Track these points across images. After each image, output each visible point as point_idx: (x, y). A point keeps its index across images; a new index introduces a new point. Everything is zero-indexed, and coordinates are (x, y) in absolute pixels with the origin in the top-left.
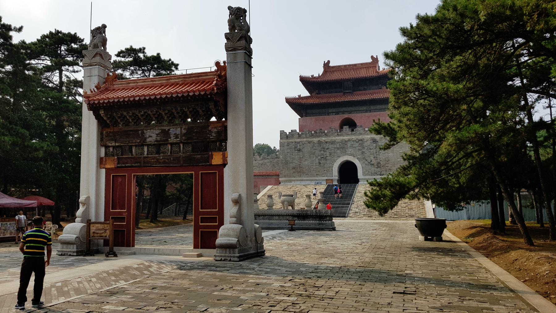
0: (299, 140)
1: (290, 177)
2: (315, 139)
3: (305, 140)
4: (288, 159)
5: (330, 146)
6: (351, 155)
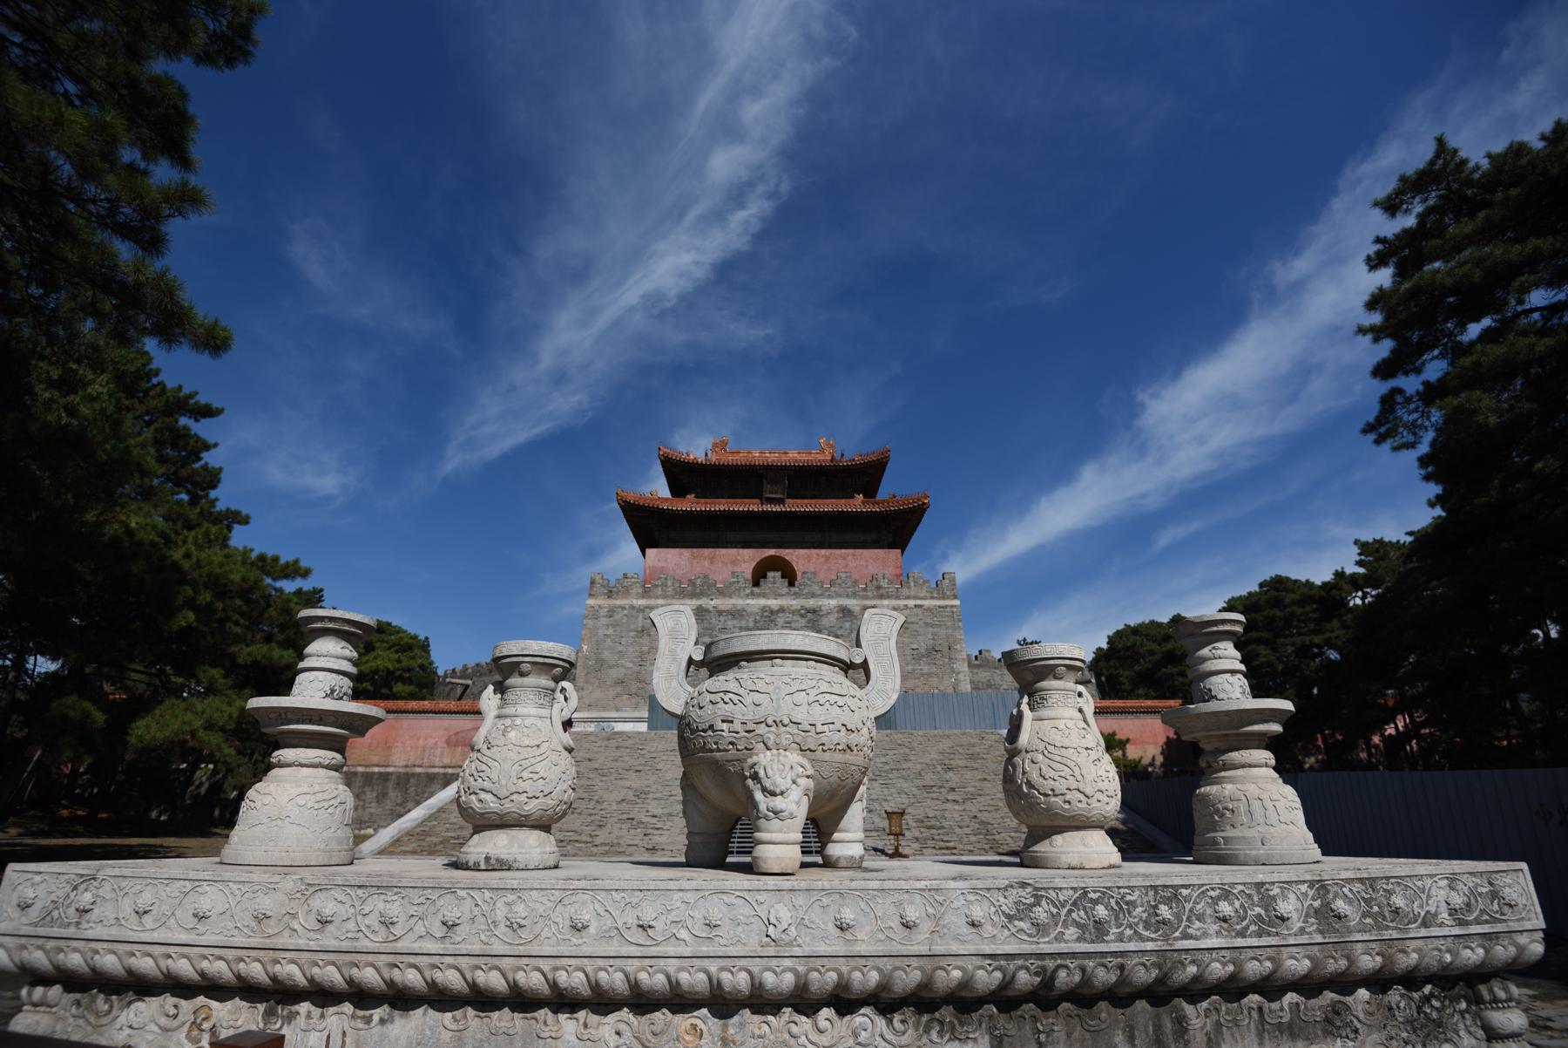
0: (642, 602)
1: (605, 708)
4: (606, 654)
5: (729, 623)
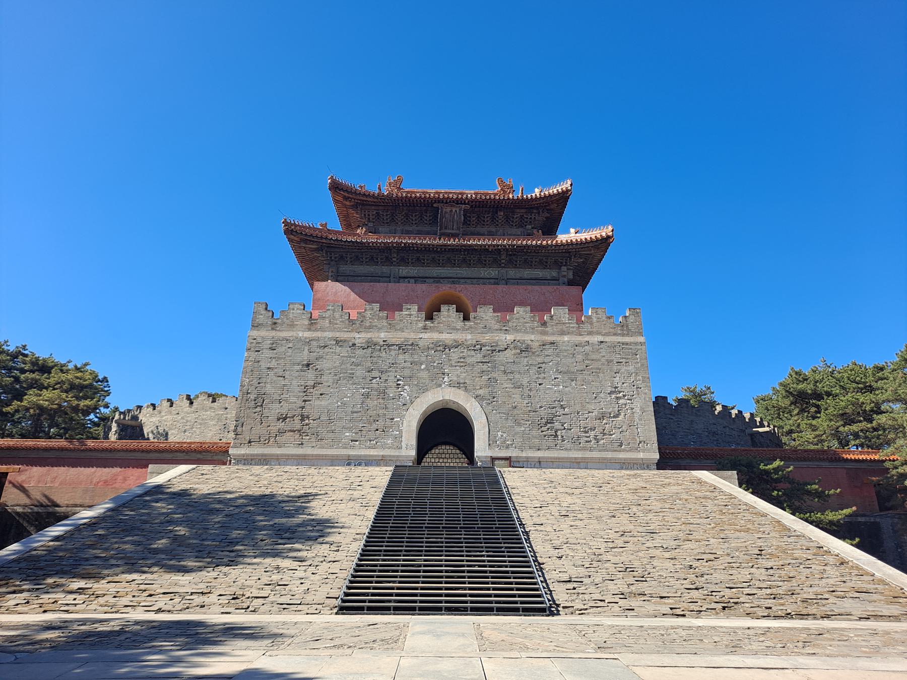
0: (308, 334)
2: (357, 335)
4: (269, 388)
6: (459, 388)
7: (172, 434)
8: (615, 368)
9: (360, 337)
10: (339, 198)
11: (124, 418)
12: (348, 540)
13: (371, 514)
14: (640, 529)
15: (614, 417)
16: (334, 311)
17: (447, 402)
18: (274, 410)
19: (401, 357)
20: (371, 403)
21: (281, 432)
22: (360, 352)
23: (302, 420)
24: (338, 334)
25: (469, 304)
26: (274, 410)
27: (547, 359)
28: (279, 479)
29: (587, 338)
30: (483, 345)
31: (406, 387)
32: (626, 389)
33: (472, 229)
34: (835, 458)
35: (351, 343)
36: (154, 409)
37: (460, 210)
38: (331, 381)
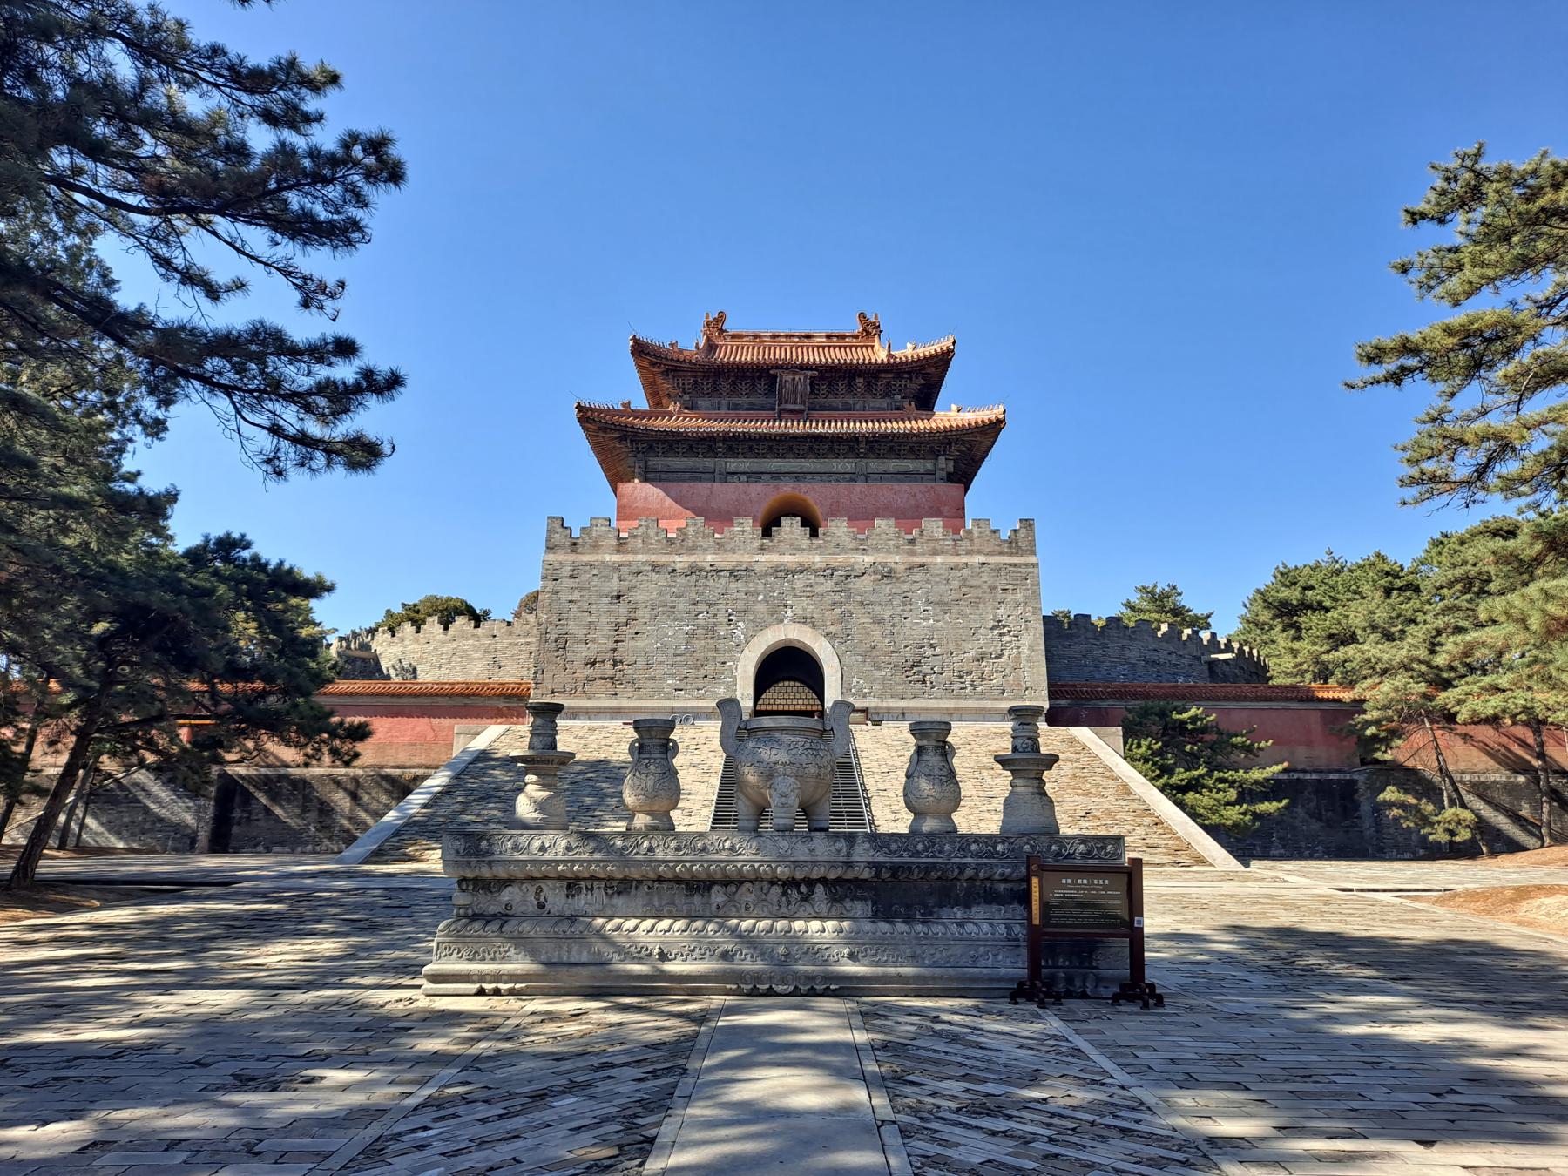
0: (616, 558)
2: (677, 559)
3: (642, 558)
4: (572, 627)
6: (805, 623)
7: (423, 670)
8: (999, 597)
9: (681, 561)
10: (645, 364)
11: (348, 647)
12: (698, 806)
13: (716, 781)
14: (981, 794)
15: (996, 658)
16: (647, 527)
17: (791, 640)
18: (580, 653)
19: (733, 586)
20: (699, 644)
21: (590, 680)
22: (681, 580)
23: (615, 665)
24: (653, 558)
25: (819, 511)
26: (580, 653)
27: (914, 587)
28: (608, 742)
29: (965, 560)
30: (834, 569)
31: (740, 624)
32: (1011, 622)
33: (821, 401)
34: (1307, 697)
35: (670, 569)
36: (393, 635)
37: (805, 378)
38: (648, 616)
